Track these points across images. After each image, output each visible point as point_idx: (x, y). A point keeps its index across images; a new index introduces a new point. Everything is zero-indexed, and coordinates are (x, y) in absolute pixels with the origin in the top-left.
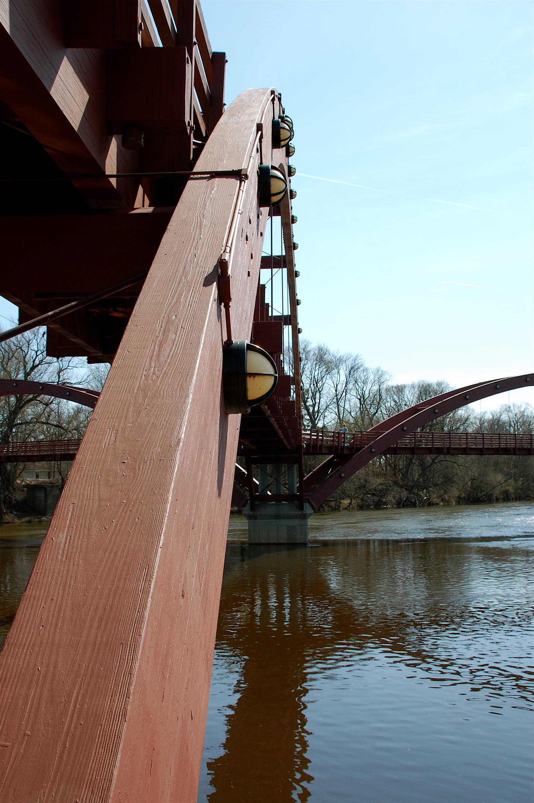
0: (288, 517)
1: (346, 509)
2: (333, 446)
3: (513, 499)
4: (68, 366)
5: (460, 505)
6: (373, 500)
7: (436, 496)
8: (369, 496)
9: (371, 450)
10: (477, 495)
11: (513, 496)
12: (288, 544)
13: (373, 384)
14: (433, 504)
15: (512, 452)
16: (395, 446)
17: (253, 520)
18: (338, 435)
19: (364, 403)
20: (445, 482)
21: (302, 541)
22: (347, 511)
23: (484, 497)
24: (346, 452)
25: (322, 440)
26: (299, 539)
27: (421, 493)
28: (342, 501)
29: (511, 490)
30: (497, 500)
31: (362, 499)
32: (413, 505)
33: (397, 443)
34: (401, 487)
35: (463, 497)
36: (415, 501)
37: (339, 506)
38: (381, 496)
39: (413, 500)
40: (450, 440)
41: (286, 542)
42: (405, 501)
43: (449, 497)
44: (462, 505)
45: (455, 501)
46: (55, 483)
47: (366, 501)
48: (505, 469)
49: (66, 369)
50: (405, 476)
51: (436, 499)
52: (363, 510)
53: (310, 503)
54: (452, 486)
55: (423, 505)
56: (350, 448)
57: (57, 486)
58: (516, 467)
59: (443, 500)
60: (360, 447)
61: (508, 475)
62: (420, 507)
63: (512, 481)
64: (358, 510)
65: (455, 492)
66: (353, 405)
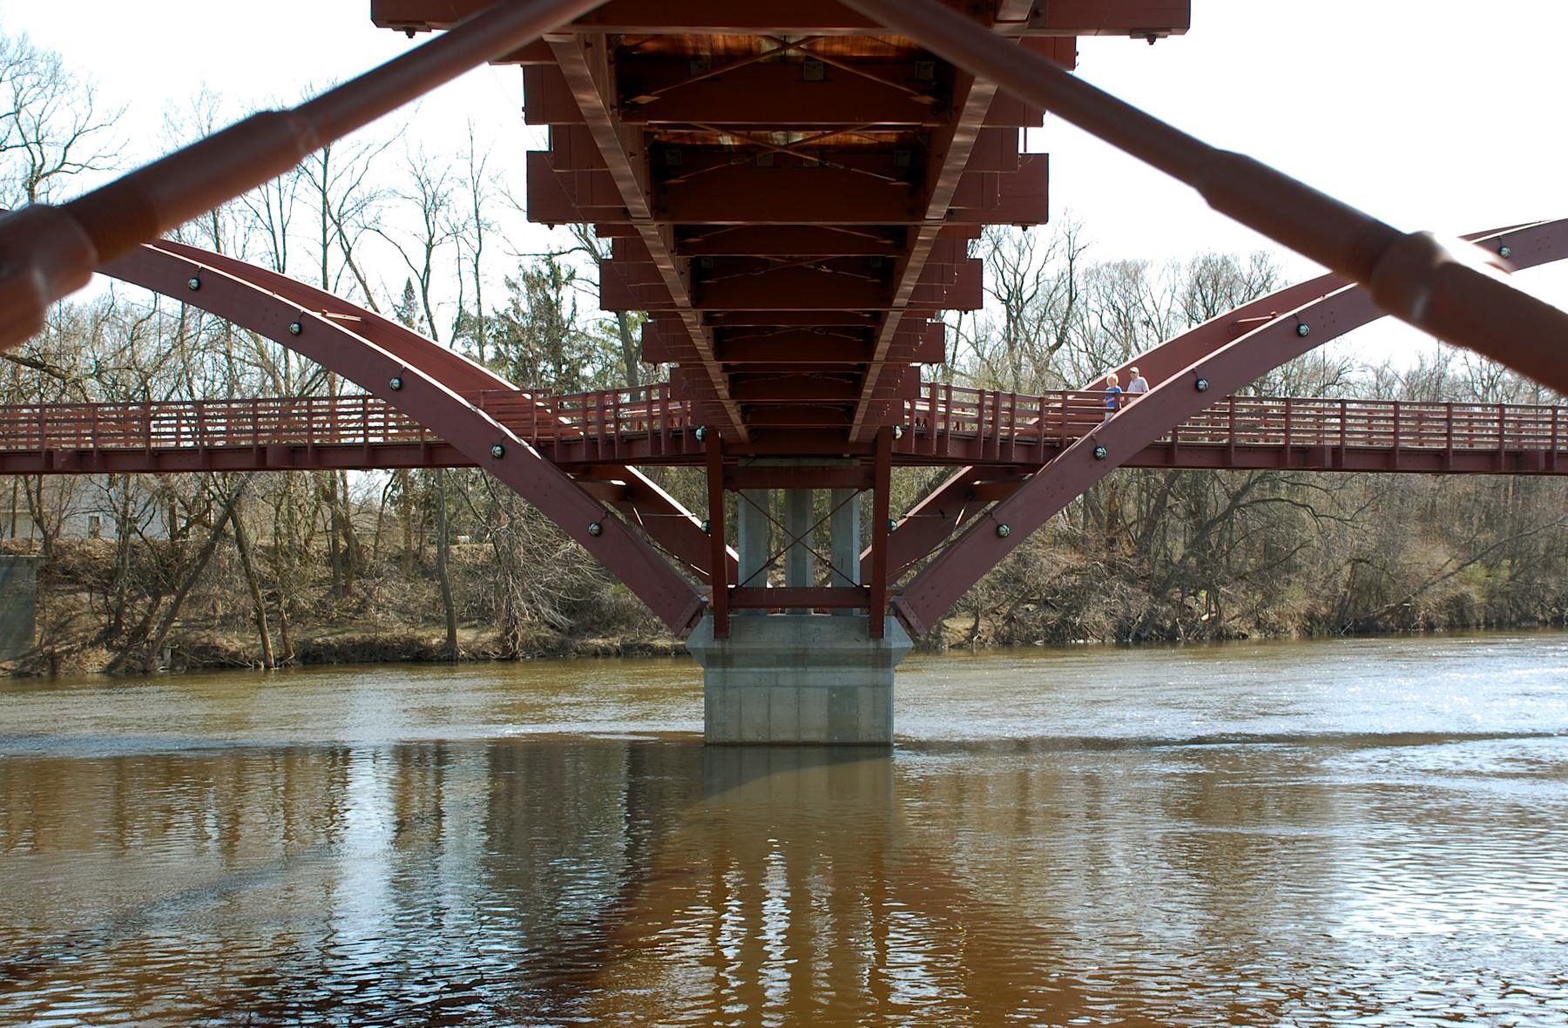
0: (834, 660)
1: (959, 646)
2: (977, 436)
3: (1478, 625)
4: (63, 164)
5: (1312, 639)
6: (1044, 620)
7: (1236, 611)
8: (1031, 607)
9: (1095, 451)
10: (1366, 609)
11: (1481, 617)
12: (830, 745)
13: (1051, 253)
14: (1229, 637)
15: (1542, 465)
16: (1169, 440)
17: (719, 670)
18: (992, 401)
19: (1018, 316)
20: (1270, 567)
21: (882, 738)
22: (962, 653)
23: (1389, 617)
24: (1017, 456)
25: (946, 417)
26: (866, 730)
27: (1190, 601)
28: (946, 622)
29: (1476, 597)
30: (1430, 629)
31: (1010, 619)
32: (1167, 638)
33: (1175, 430)
34: (1131, 581)
35: (1323, 616)
36: (1175, 625)
37: (938, 637)
38: (1069, 610)
39: (1168, 624)
40: (1343, 424)
41: (822, 737)
42: (1144, 625)
43: (1279, 614)
44: (1319, 639)
45: (1300, 629)
46: (21, 553)
47: (1021, 623)
48: (1457, 529)
49: (56, 171)
50: (1142, 548)
51: (1238, 620)
52: (1011, 651)
53: (899, 614)
54: (1289, 583)
55: (1199, 640)
56: (1030, 446)
57: (30, 561)
58: (1490, 521)
59: (1258, 625)
60: (1061, 442)
61: (1470, 552)
62: (1188, 644)
63: (1478, 571)
64: (996, 651)
65: (1297, 600)
66: (983, 323)
